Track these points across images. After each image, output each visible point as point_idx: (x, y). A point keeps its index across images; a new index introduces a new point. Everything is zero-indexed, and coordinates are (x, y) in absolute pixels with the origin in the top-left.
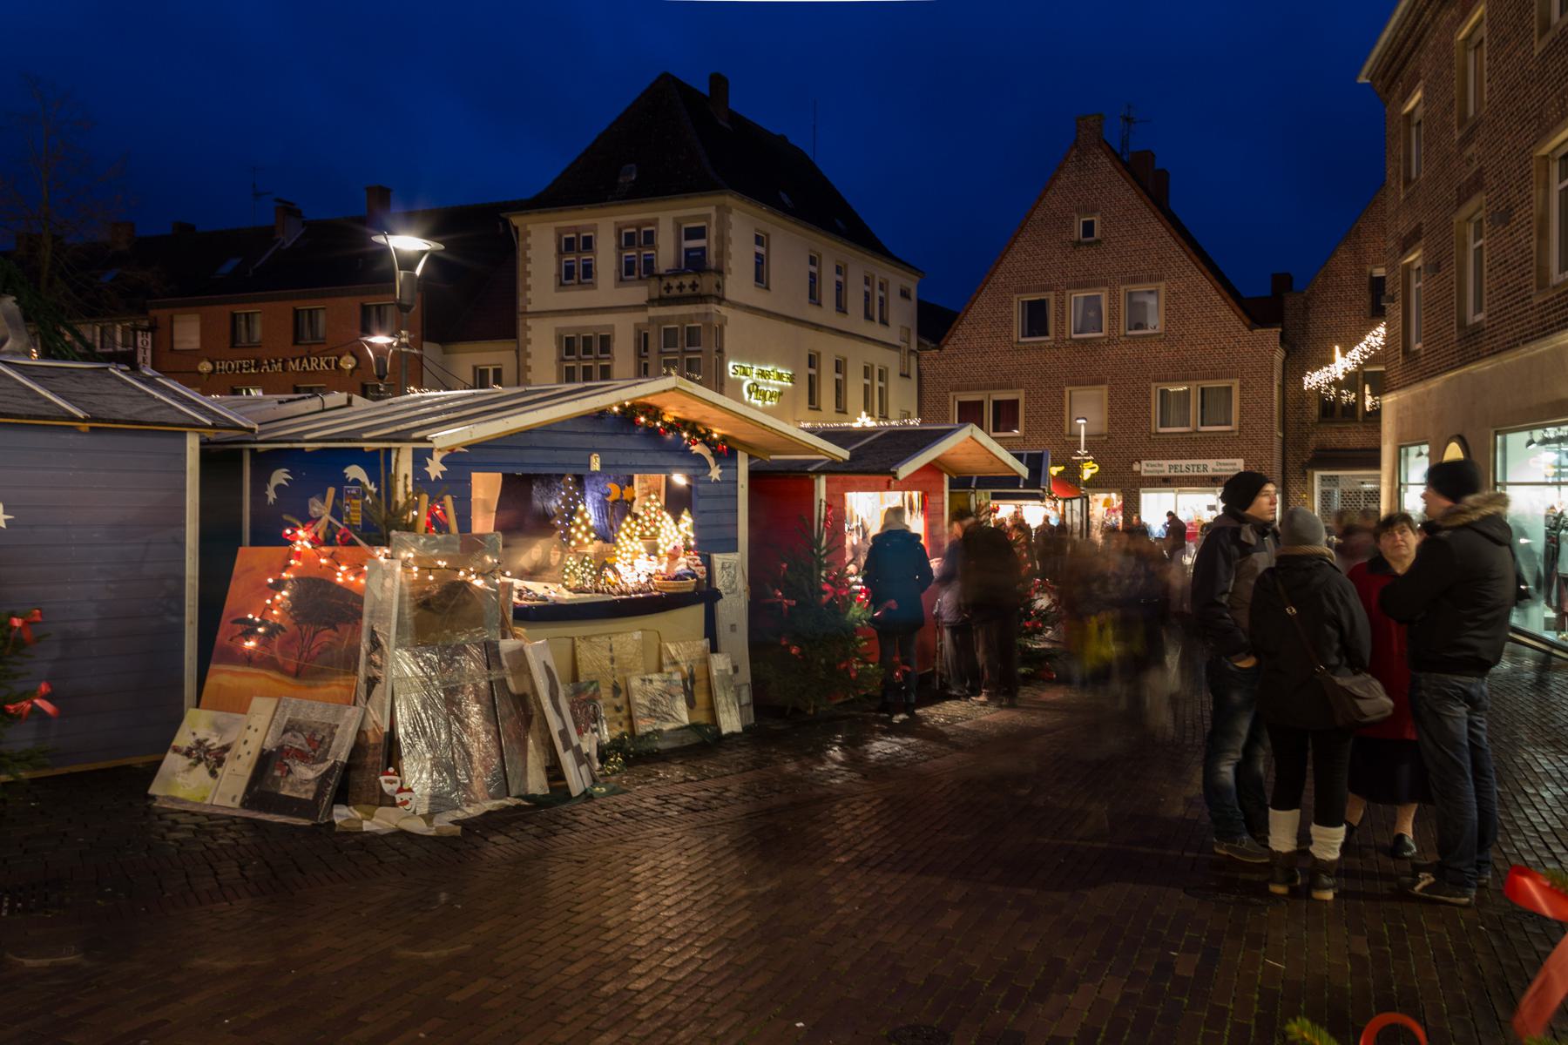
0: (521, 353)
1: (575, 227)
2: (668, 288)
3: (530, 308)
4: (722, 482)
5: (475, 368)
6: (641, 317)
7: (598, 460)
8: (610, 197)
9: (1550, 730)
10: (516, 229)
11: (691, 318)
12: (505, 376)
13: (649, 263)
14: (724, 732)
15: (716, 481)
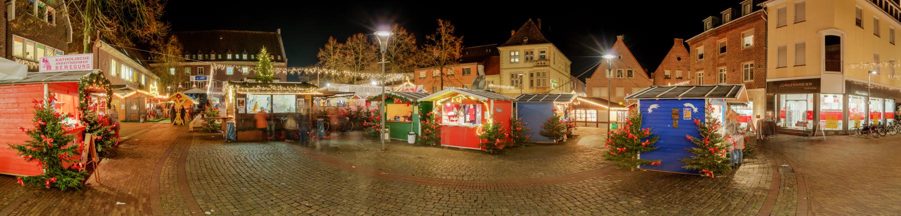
2: (538, 64)
6: (531, 70)
11: (544, 70)
13: (532, 58)
14: (812, 120)
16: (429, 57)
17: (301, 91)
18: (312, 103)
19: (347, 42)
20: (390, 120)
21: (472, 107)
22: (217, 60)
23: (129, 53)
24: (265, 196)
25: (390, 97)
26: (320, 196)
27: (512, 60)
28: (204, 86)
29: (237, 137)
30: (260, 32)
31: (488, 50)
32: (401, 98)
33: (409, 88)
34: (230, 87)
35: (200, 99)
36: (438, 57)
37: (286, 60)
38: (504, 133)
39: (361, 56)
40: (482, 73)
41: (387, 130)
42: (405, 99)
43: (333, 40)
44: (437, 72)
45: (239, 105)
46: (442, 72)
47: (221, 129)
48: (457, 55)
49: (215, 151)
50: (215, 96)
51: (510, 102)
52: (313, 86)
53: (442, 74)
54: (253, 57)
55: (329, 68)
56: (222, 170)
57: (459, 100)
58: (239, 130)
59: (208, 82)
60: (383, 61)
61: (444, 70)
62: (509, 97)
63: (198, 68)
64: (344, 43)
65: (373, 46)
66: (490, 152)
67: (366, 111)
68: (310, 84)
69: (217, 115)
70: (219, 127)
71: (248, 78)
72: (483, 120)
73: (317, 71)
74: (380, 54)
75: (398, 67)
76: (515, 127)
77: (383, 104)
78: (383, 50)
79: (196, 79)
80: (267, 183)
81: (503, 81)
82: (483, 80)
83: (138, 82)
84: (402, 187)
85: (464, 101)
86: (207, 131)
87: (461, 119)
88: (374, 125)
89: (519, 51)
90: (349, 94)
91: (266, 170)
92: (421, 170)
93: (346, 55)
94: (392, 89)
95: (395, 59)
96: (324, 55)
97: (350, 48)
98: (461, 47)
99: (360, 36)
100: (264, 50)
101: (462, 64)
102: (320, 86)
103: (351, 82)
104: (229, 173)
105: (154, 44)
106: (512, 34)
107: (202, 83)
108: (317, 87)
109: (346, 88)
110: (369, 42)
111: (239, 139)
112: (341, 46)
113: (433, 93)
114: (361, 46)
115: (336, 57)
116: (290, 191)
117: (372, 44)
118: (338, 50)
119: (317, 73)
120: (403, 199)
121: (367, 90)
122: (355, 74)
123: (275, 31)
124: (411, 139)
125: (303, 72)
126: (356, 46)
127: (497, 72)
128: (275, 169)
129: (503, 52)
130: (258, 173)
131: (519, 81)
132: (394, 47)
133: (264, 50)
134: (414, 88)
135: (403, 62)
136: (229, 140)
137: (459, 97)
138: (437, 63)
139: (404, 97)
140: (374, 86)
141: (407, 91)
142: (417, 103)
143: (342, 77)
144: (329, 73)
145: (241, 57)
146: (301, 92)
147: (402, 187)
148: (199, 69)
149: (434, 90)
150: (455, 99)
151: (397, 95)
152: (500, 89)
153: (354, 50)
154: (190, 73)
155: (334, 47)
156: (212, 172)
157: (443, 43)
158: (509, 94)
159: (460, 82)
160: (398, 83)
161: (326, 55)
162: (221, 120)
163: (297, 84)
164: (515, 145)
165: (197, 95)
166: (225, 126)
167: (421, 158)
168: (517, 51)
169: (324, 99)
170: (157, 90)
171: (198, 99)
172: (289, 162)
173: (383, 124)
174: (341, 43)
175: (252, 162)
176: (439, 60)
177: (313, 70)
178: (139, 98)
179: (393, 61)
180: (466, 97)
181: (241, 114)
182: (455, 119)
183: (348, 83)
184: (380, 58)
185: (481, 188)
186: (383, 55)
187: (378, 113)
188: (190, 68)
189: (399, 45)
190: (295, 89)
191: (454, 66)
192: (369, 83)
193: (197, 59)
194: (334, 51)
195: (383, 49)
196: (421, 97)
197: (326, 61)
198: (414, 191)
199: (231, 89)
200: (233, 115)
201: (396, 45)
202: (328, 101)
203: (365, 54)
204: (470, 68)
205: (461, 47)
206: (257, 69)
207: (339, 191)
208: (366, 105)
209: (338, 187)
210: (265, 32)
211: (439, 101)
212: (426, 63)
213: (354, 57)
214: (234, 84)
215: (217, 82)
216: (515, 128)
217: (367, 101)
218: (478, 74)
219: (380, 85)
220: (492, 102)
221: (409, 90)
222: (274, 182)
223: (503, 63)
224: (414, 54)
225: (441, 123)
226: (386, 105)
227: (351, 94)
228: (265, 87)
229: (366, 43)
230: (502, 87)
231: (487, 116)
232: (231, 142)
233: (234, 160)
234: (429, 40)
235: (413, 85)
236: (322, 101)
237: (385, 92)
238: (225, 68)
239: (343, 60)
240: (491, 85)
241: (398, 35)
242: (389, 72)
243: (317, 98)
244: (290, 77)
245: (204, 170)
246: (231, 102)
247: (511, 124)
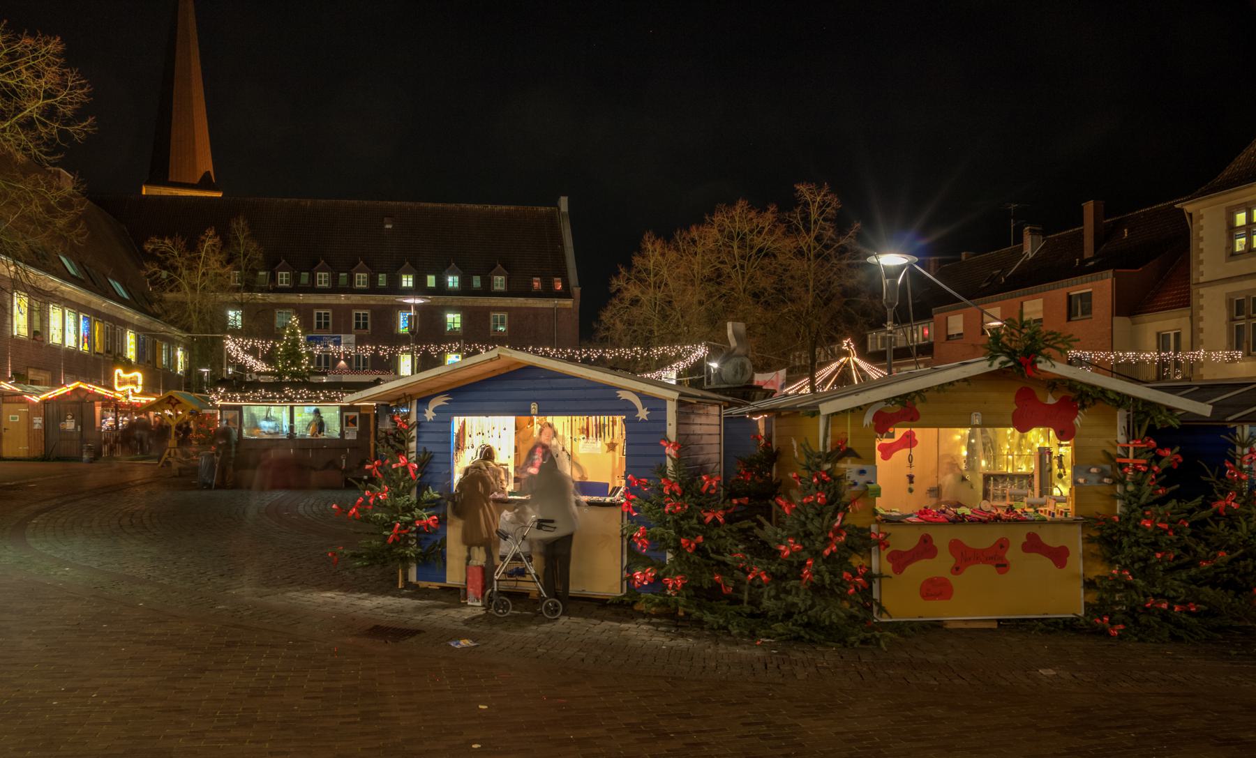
0: (1194, 318)
1: (1246, 203)
3: (1202, 279)
4: (649, 421)
5: (1158, 334)
7: (536, 407)
9: (174, 575)
15: (643, 420)
23: (80, 264)
27: (1240, 243)
30: (504, 207)
37: (577, 291)
45: (347, 425)
63: (354, 312)
81: (1201, 330)
83: (108, 352)
105: (154, 250)
145: (487, 283)
148: (319, 316)
170: (140, 381)
178: (81, 402)
204: (1091, 292)
210: (521, 208)
223: (1201, 262)
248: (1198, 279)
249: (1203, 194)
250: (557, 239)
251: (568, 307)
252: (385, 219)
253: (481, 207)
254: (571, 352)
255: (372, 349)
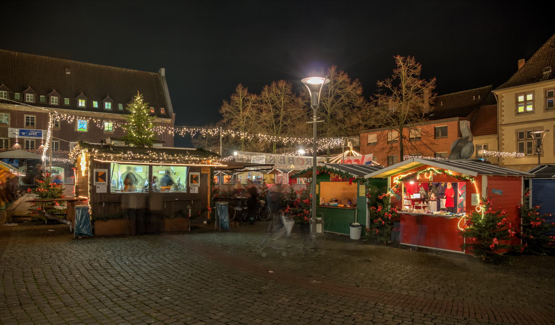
1: (524, 92)
3: (503, 123)
8: (541, 80)
10: (497, 96)
12: (489, 148)
16: (382, 113)
17: (195, 161)
18: (212, 178)
19: (263, 93)
20: (324, 205)
21: (449, 186)
22: (61, 106)
24: (138, 318)
25: (324, 172)
26: (221, 314)
27: (521, 109)
28: (37, 148)
29: (93, 230)
30: (132, 70)
31: (476, 97)
32: (340, 173)
33: (351, 158)
34: (83, 151)
35: (29, 169)
36: (396, 113)
37: (174, 115)
38: (506, 230)
39: (283, 113)
40: (466, 133)
41: (320, 219)
42: (346, 174)
43: (243, 89)
44: (394, 135)
45: (97, 180)
46: (401, 135)
47: (65, 219)
48: (426, 107)
49: (53, 255)
50: (55, 164)
51: (519, 179)
52: (214, 154)
53: (402, 137)
54: (121, 107)
55: (236, 130)
56: (66, 285)
57: (428, 175)
58: (98, 219)
59: (45, 141)
60: (315, 119)
61: (405, 131)
62: (517, 171)
63: (25, 116)
64: (259, 93)
65: (300, 99)
66: (481, 258)
67: (289, 191)
68: (209, 152)
69: (59, 195)
70: (63, 215)
71: (112, 139)
72: (470, 207)
73: (219, 132)
74: (310, 110)
75: (336, 129)
76: (527, 220)
77: (315, 182)
78: (314, 105)
79: (21, 135)
80: (141, 298)
82: (469, 144)
84: (341, 303)
85: (435, 177)
86: (39, 221)
87: (433, 205)
88: (301, 212)
89: (533, 93)
90: (265, 168)
91: (139, 279)
92: (370, 279)
93: (261, 111)
94: (328, 160)
95: (331, 117)
96: (230, 110)
97: (266, 101)
98: (433, 96)
99: (282, 84)
100: (139, 98)
101: (433, 121)
102: (223, 153)
103: (268, 150)
104: (79, 288)
106: (520, 66)
107: (32, 142)
108: (219, 156)
109: (261, 159)
110: (294, 94)
111: (97, 232)
112: (254, 97)
113: (388, 166)
114: (282, 98)
115: (247, 114)
116: (176, 308)
117: (298, 95)
118: (250, 104)
119: (219, 136)
120: (343, 320)
121: (291, 161)
122: (274, 139)
123: (157, 70)
124: (354, 233)
125: (198, 134)
126: (275, 98)
127: (493, 130)
128: (154, 277)
129: (503, 97)
130: (127, 283)
131: (534, 143)
132: (330, 100)
133: (139, 98)
134: (360, 159)
135: (342, 121)
136: (81, 234)
137: (428, 172)
138: (394, 120)
139: (344, 172)
140: (301, 155)
141: (349, 163)
142: (363, 181)
143: (256, 142)
144: (236, 136)
146: (196, 163)
147: (341, 303)
149: (389, 161)
150: (422, 175)
151: (334, 168)
152: (499, 158)
153: (272, 104)
154: (8, 123)
155: (243, 100)
156: (48, 289)
157: (404, 91)
158: (515, 165)
159: (430, 148)
160: (337, 151)
161: (232, 110)
162: (66, 204)
163: (189, 151)
164: (527, 251)
165: (21, 162)
166: (73, 213)
167: (370, 261)
168: (529, 93)
169: (229, 174)
171: (24, 167)
172: (176, 265)
173: (313, 210)
174: (254, 94)
175: (118, 269)
176: (396, 117)
177: (214, 131)
179: (329, 120)
180: (439, 171)
181: (101, 194)
182: (421, 205)
183: (264, 152)
184: (310, 115)
185: (466, 315)
186: (315, 111)
187: (306, 194)
188: (9, 115)
189: (337, 97)
190: (187, 159)
191: (420, 125)
192: (295, 151)
193: (23, 101)
194: (243, 104)
195: (314, 103)
196: (370, 172)
197: (232, 119)
198: (358, 310)
199: (84, 154)
200: (87, 195)
201: (333, 96)
202: (235, 176)
203: (289, 110)
204: (447, 127)
205: (433, 96)
206: (128, 126)
207: (250, 307)
208: (290, 183)
209: (248, 301)
210: (140, 72)
211: (397, 177)
212: (377, 121)
213: (272, 114)
214: (90, 147)
215: (61, 142)
216: (529, 222)
217: (291, 178)
218: (460, 135)
219: (310, 155)
220: (484, 179)
221: (353, 161)
222: (153, 297)
224: (359, 108)
225: (399, 210)
226: (318, 183)
227: (268, 168)
228: (140, 154)
229: (291, 95)
230: (502, 154)
231: (476, 201)
232: (83, 238)
233: (88, 267)
234: (381, 88)
235: (358, 154)
236: (226, 176)
237: (318, 165)
238: (75, 120)
239: (258, 118)
240: (483, 152)
241: (335, 82)
242: (323, 136)
243: (220, 172)
244: (178, 140)
245: (33, 287)
246: (83, 174)
247: (520, 216)
248: (502, 123)
249: (504, 87)
250: (160, 89)
251: (169, 123)
252: (66, 69)
253: (119, 69)
254: (281, 139)
255: (163, 129)
